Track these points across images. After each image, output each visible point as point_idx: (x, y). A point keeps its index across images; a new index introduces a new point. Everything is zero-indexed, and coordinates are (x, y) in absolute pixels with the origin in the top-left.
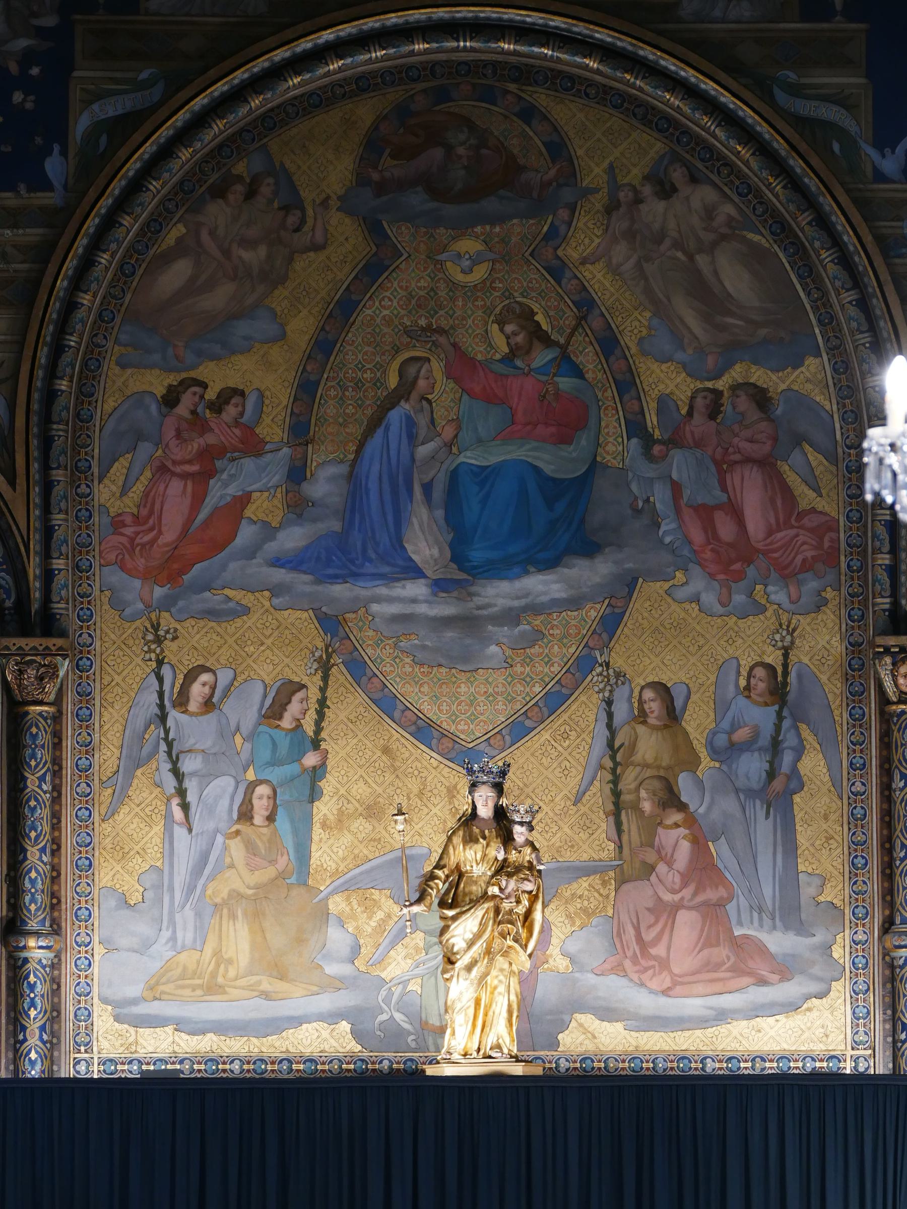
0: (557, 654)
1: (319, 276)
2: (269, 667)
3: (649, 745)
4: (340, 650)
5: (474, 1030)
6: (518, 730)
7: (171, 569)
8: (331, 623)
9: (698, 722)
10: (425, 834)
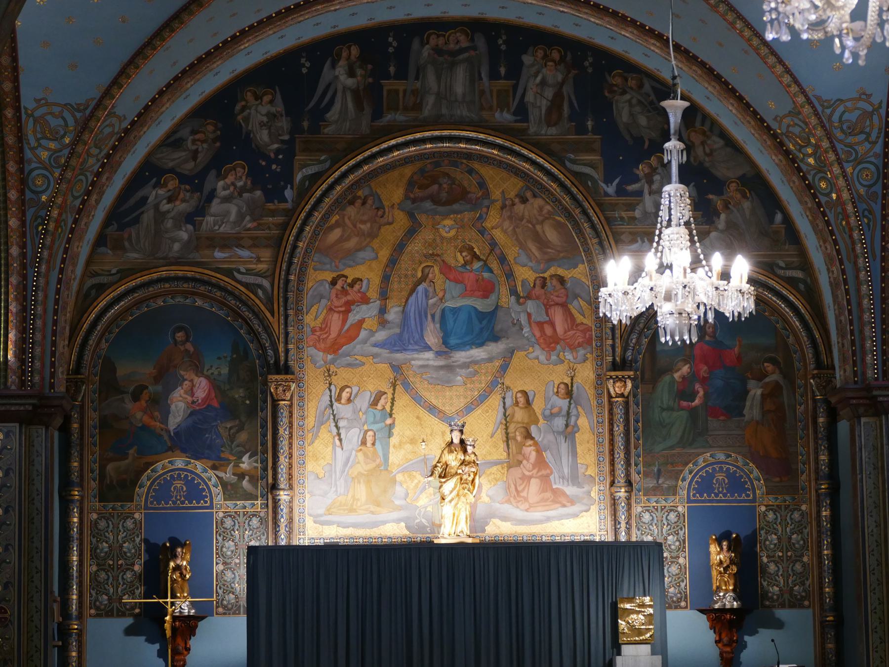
0: (483, 381)
1: (391, 234)
2: (372, 386)
3: (520, 415)
4: (399, 378)
5: (453, 528)
6: (469, 409)
7: (334, 348)
8: (396, 368)
9: (538, 406)
10: (433, 449)
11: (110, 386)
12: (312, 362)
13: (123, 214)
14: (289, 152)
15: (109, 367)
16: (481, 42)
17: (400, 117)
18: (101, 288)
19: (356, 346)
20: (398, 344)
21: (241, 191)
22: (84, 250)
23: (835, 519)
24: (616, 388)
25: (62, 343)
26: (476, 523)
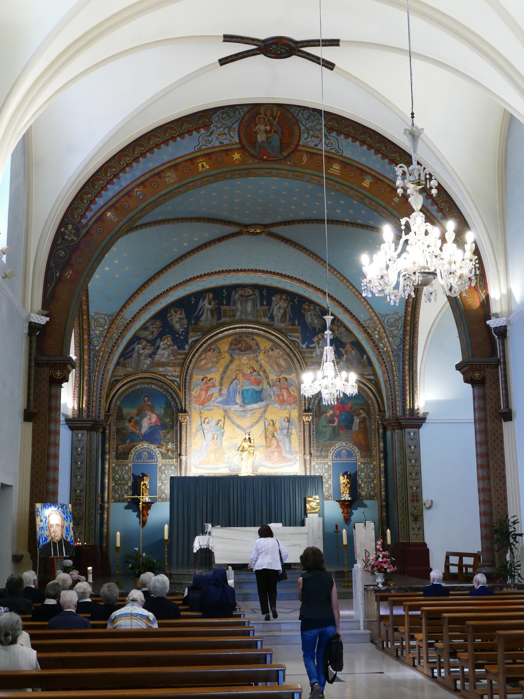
0: (257, 416)
1: (224, 362)
3: (270, 428)
5: (245, 471)
6: (252, 426)
7: (203, 404)
8: (225, 411)
9: (277, 425)
11: (120, 417)
12: (194, 409)
13: (126, 354)
14: (187, 332)
15: (120, 410)
16: (257, 293)
17: (228, 320)
18: (117, 381)
19: (211, 403)
20: (226, 402)
21: (170, 345)
22: (111, 367)
23: (386, 467)
24: (306, 419)
25: (103, 401)
26: (254, 468)
